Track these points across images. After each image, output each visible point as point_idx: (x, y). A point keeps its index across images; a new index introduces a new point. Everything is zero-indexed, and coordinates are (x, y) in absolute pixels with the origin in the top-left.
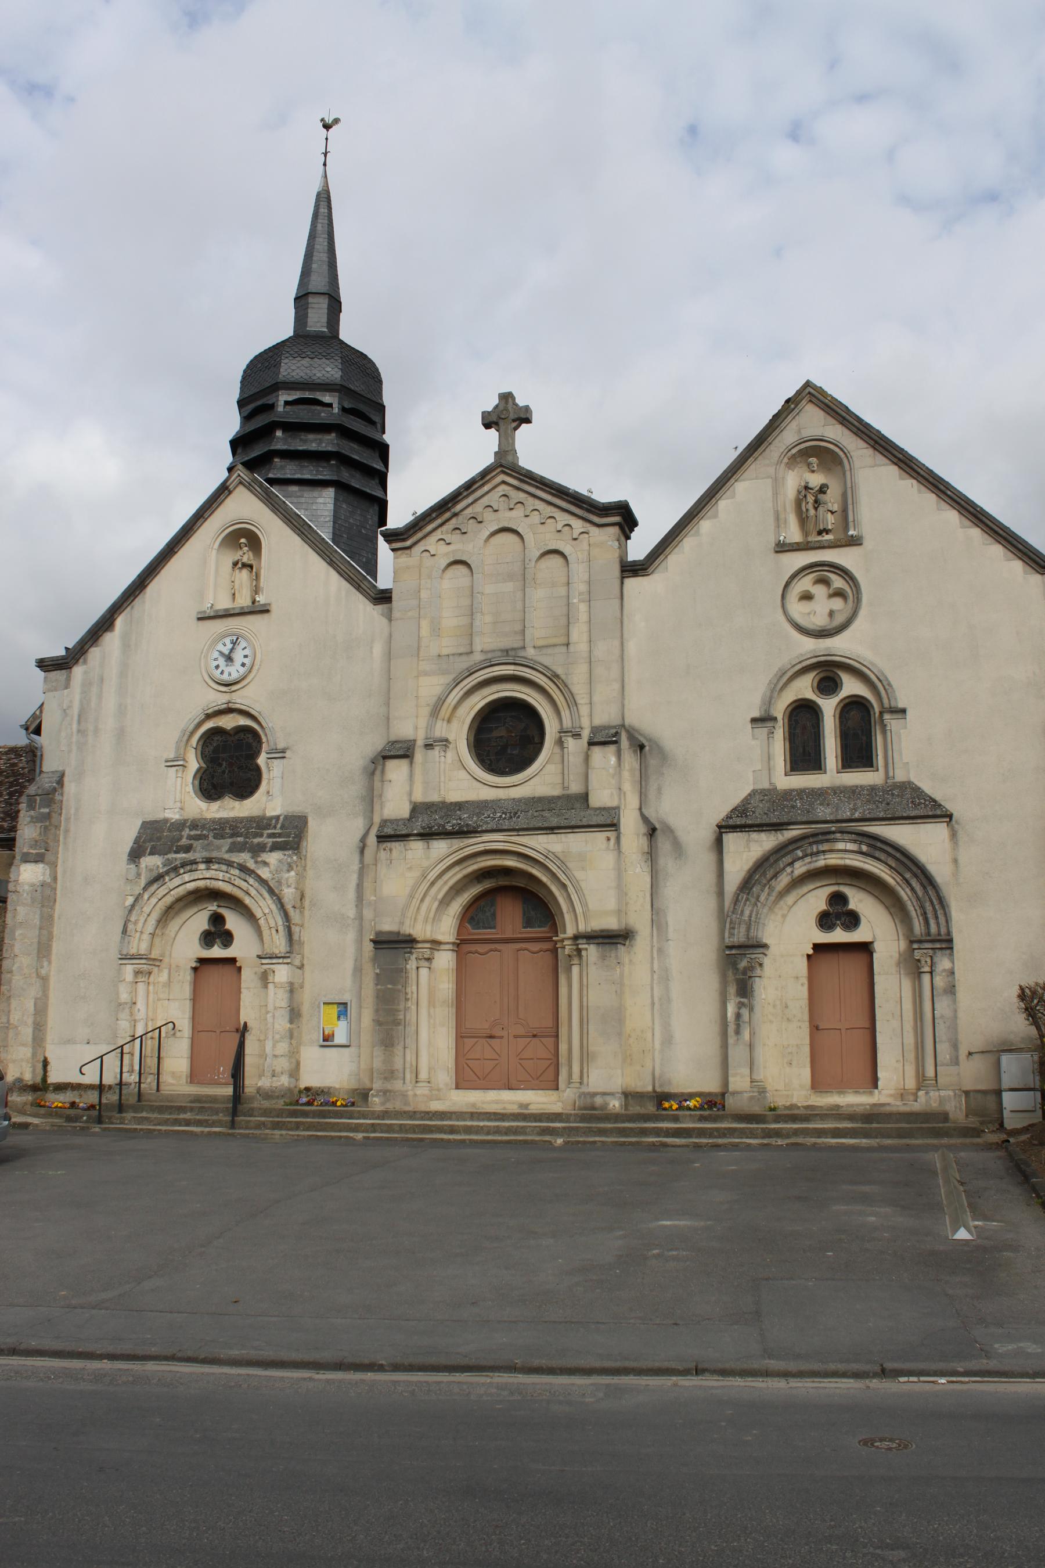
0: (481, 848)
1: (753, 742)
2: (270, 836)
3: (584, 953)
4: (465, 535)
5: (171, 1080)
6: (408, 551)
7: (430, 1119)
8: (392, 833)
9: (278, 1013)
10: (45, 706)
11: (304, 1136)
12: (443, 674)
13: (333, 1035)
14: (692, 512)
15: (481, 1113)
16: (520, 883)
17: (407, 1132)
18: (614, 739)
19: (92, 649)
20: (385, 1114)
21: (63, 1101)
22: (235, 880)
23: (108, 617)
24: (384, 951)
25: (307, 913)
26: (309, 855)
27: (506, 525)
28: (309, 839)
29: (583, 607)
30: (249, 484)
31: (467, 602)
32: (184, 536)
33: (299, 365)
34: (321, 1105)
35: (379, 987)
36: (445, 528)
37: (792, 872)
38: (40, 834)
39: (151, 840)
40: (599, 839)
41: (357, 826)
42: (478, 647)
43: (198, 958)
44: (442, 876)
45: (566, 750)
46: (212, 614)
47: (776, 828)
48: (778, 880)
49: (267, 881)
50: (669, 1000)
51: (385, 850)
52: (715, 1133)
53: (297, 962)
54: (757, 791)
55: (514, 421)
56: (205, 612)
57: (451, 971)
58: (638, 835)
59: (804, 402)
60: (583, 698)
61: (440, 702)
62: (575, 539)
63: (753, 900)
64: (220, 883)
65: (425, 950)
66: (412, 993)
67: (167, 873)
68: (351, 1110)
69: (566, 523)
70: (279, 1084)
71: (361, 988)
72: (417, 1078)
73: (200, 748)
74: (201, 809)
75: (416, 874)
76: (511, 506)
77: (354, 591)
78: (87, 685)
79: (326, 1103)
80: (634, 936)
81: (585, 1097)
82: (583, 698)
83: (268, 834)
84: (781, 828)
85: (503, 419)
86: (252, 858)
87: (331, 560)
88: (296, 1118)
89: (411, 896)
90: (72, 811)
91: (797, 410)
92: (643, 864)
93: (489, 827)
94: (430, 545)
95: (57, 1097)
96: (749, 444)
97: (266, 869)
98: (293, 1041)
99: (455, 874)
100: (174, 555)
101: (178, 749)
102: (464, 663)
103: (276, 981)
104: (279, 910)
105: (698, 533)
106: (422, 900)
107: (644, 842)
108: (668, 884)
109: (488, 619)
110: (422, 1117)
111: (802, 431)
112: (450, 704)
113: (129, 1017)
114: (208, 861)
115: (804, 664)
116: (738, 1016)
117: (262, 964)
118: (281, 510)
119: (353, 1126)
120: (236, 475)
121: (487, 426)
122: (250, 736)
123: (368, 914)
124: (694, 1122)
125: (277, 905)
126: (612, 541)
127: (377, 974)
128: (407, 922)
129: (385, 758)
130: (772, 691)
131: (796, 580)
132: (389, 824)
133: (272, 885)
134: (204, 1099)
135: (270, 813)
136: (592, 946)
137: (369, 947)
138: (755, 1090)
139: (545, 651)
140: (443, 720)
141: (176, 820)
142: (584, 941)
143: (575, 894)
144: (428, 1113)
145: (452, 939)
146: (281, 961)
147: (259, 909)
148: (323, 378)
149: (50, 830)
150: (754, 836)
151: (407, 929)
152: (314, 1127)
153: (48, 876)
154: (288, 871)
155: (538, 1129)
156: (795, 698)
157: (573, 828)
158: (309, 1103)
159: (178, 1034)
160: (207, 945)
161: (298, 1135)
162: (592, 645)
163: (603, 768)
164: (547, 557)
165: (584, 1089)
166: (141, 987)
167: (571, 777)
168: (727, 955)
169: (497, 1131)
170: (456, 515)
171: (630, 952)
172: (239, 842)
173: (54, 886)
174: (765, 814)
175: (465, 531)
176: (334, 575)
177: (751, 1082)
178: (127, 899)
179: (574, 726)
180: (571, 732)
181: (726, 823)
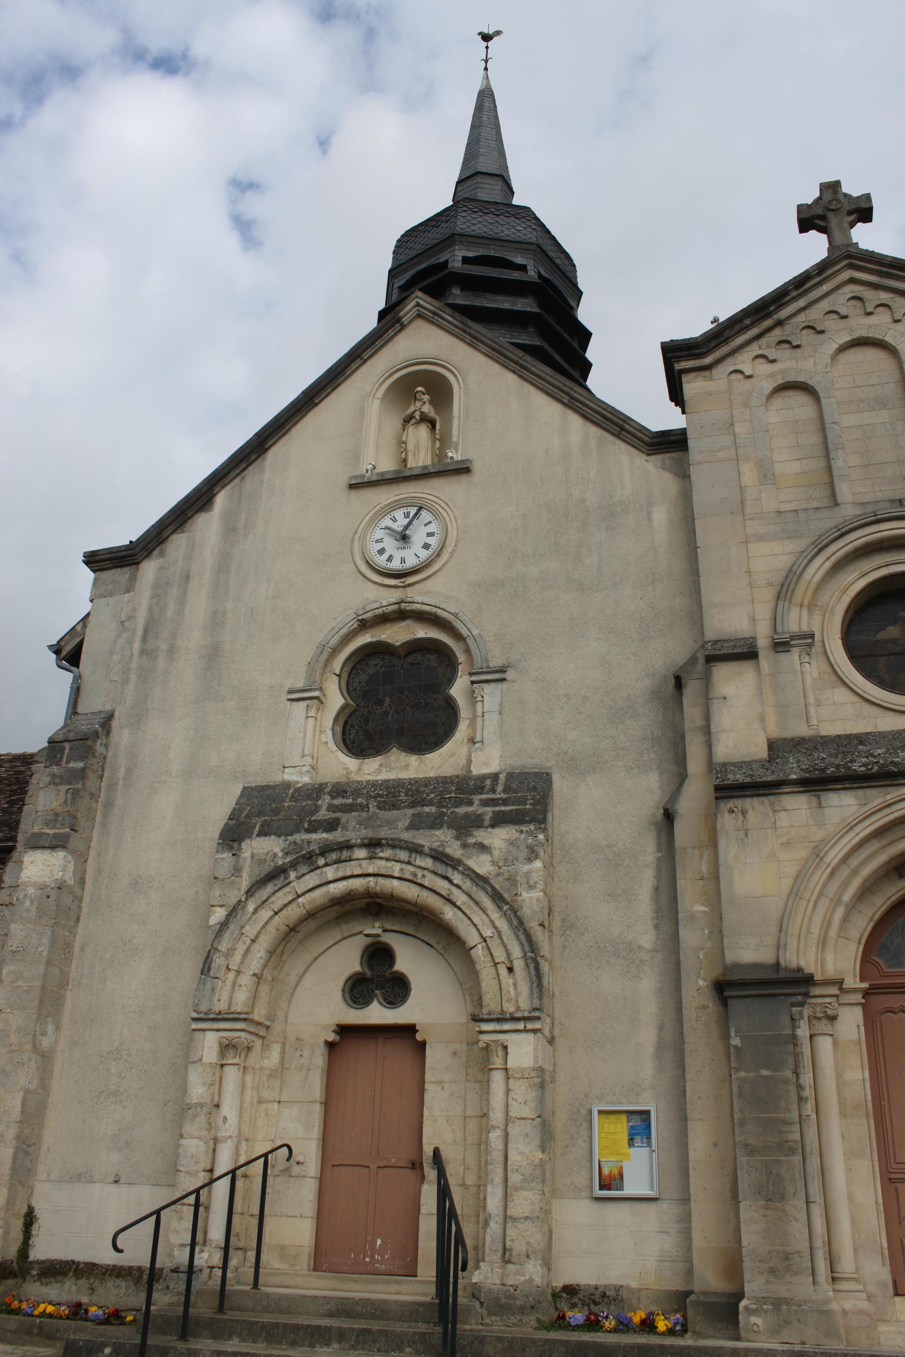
2: (485, 803)
4: (798, 351)
5: (277, 1264)
6: (707, 373)
8: (748, 780)
10: (90, 618)
12: (789, 538)
13: (621, 1175)
19: (175, 537)
21: (56, 1300)
22: (424, 876)
23: (205, 489)
27: (864, 333)
30: (434, 313)
31: (815, 439)
32: (331, 381)
33: (480, 220)
36: (764, 341)
38: (65, 802)
39: (259, 815)
42: (845, 492)
43: (338, 1025)
46: (374, 478)
55: (850, 213)
56: (363, 476)
64: (395, 883)
65: (827, 1000)
67: (294, 865)
70: (522, 1278)
72: (832, 1272)
73: (345, 676)
74: (347, 769)
75: (801, 853)
76: (869, 310)
77: (611, 438)
78: (160, 588)
83: (481, 800)
86: (457, 838)
87: (572, 397)
90: (122, 773)
95: (44, 1290)
97: (485, 858)
100: (313, 407)
101: (310, 673)
102: (827, 521)
113: (204, 1133)
114: (373, 844)
117: (481, 1032)
118: (485, 340)
120: (413, 303)
121: (805, 224)
122: (433, 657)
128: (792, 945)
129: (711, 659)
133: (497, 886)
134: (358, 1309)
135: (477, 770)
140: (801, 606)
141: (305, 785)
146: (520, 1026)
147: (473, 931)
148: (513, 236)
149: (82, 797)
153: (71, 875)
154: (530, 860)
159: (296, 1170)
160: (355, 1002)
166: (232, 1075)
170: (780, 323)
172: (428, 814)
173: (79, 894)
175: (798, 343)
178: (214, 912)
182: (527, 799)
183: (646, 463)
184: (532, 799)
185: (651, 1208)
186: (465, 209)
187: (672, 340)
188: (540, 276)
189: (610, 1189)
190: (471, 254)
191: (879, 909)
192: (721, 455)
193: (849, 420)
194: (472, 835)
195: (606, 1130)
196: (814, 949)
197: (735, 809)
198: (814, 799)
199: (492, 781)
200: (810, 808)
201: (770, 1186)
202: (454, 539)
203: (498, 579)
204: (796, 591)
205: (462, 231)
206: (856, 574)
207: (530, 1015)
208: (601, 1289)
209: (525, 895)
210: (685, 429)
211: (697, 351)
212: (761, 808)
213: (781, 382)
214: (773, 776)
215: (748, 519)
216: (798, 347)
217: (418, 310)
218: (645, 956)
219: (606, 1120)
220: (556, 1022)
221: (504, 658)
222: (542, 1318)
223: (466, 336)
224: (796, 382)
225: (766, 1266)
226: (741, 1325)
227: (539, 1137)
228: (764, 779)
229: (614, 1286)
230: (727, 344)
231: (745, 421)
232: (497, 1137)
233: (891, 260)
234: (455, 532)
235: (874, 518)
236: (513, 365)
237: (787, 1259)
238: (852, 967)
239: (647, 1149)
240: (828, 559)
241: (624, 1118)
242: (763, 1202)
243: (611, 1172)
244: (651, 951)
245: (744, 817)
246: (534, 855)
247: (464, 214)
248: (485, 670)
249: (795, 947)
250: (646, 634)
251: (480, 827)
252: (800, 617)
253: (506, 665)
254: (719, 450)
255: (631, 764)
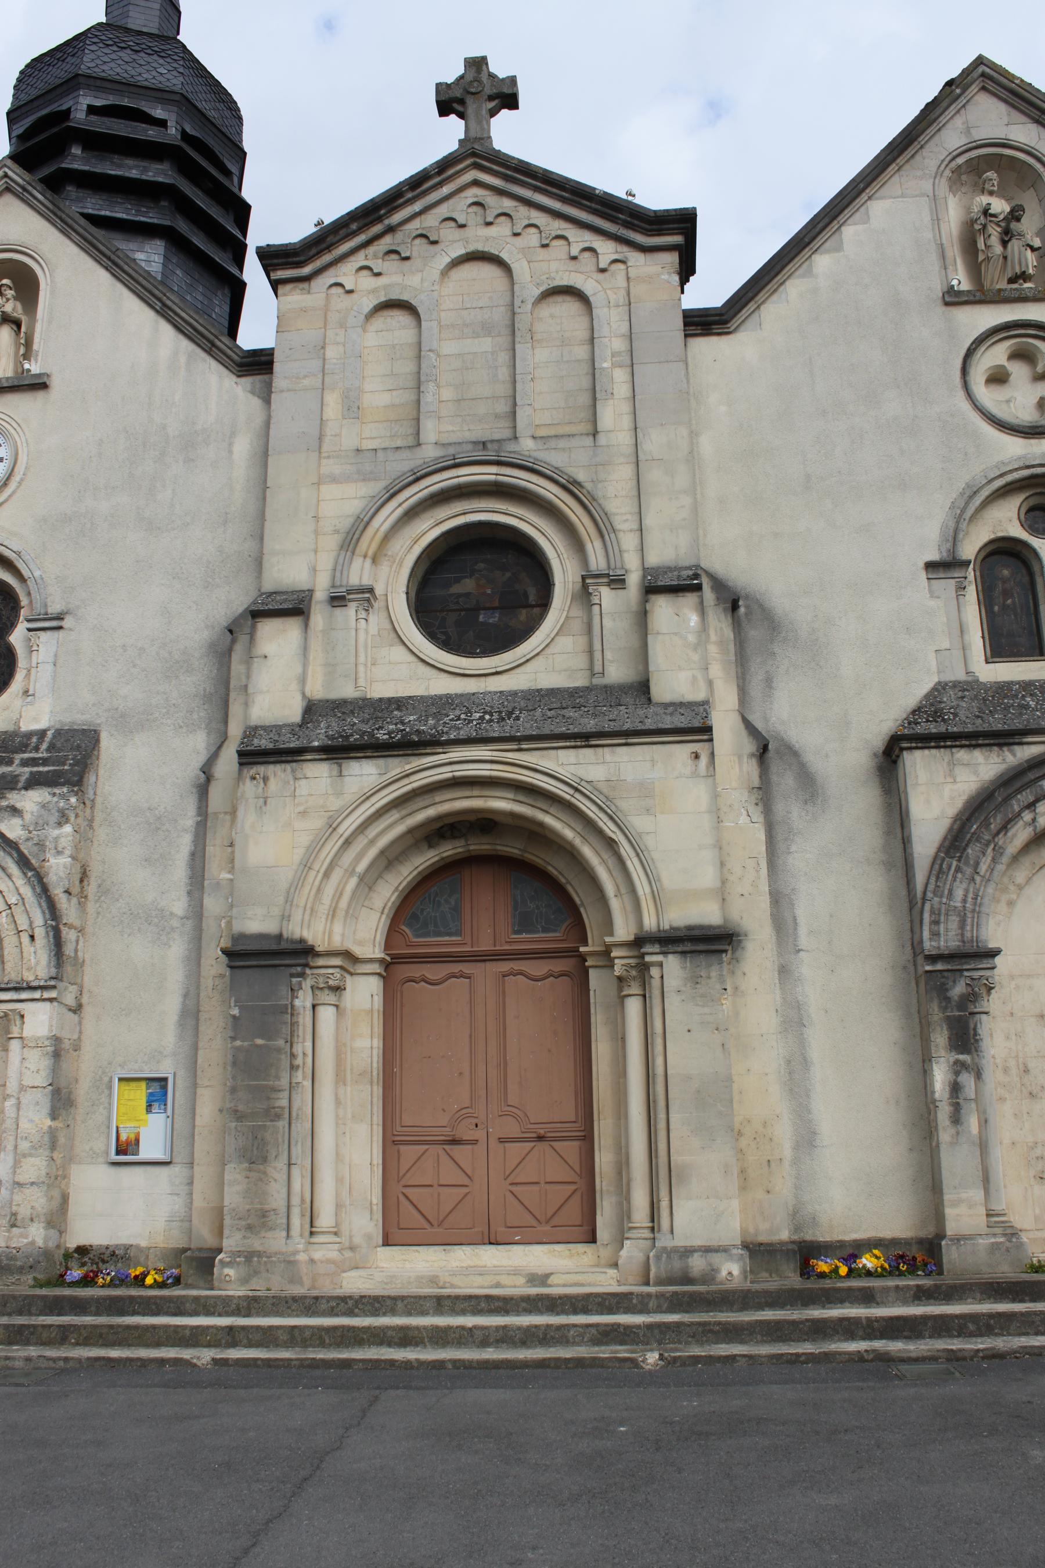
0: (445, 773)
1: (932, 603)
2: (25, 763)
3: (655, 972)
4: (407, 263)
6: (305, 285)
7: (350, 1313)
8: (271, 746)
9: (27, 1098)
11: (79, 1360)
12: (364, 480)
13: (137, 1141)
14: (802, 239)
15: (457, 1297)
16: (511, 848)
17: (305, 1344)
18: (695, 582)
20: (251, 1305)
24: (249, 971)
25: (91, 907)
26: (99, 800)
27: (480, 247)
28: (101, 772)
29: (620, 376)
30: (24, 189)
31: (410, 367)
33: (113, 56)
34: (112, 1285)
35: (238, 1043)
36: (371, 250)
37: (1034, 820)
40: (680, 753)
41: (199, 743)
42: (430, 431)
44: (366, 828)
45: (596, 608)
47: (1001, 741)
48: (1010, 834)
49: (16, 844)
50: (806, 1063)
51: (253, 778)
52: (971, 1327)
53: (70, 999)
54: (946, 684)
55: (491, 98)
57: (376, 1015)
58: (740, 757)
59: (974, 88)
60: (627, 520)
61: (361, 524)
62: (603, 271)
63: (969, 871)
65: (330, 971)
66: (304, 1054)
68: (179, 1297)
69: (586, 245)
70: (25, 1241)
71: (195, 1048)
72: (312, 1226)
75: (317, 823)
76: (490, 219)
77: (202, 354)
79: (121, 1281)
80: (740, 941)
81: (669, 1257)
82: (627, 520)
83: (22, 759)
84: (1011, 741)
85: (473, 94)
87: (164, 304)
88: (59, 1314)
89: (306, 865)
91: (963, 100)
92: (752, 809)
93: (463, 734)
94: (345, 274)
96: (890, 144)
97: (16, 821)
98: (56, 1155)
99: (391, 826)
102: (403, 464)
103: (24, 1035)
104: (38, 896)
105: (809, 273)
106: (327, 875)
107: (752, 768)
108: (793, 848)
109: (447, 394)
110: (333, 1308)
111: (973, 131)
112: (378, 530)
115: (1009, 478)
116: (955, 1088)
118: (76, 227)
119: (187, 1332)
121: (445, 108)
123: (213, 905)
124: (905, 1302)
125: (34, 889)
126: (669, 274)
127: (234, 1017)
128: (297, 915)
130: (958, 520)
131: (983, 348)
132: (262, 732)
133: (26, 852)
135: (26, 726)
136: (671, 957)
137: (214, 964)
138: (998, 1231)
139: (553, 443)
140: (365, 557)
142: (656, 948)
143: (636, 860)
144: (344, 1299)
145: (379, 954)
146: (37, 995)
148: (154, 81)
150: (961, 754)
151: (299, 929)
152: (101, 1335)
154: (60, 824)
155: (593, 1331)
156: (993, 536)
157: (628, 736)
158: (87, 1281)
161: (66, 1359)
162: (640, 435)
163: (676, 634)
164: (551, 299)
165: (664, 1241)
167: (608, 655)
168: (927, 972)
169: (505, 1337)
170: (391, 230)
171: (733, 973)
174: (978, 717)
175: (407, 254)
176: (167, 330)
177: (988, 1215)
179: (612, 566)
180: (608, 575)
181: (911, 732)
182: (68, 760)
183: (235, 386)
184: (72, 759)
185: (163, 1171)
186: (95, 40)
187: (268, 245)
188: (184, 133)
189: (126, 1155)
190: (98, 103)
191: (405, 878)
192: (306, 382)
193: (449, 348)
194: (5, 797)
195: (126, 1097)
196: (323, 920)
197: (257, 776)
198: (335, 767)
199: (38, 739)
200: (331, 777)
201: (255, 1149)
202: (24, 467)
203: (65, 514)
204: (362, 540)
205: (88, 71)
206: (431, 522)
207: (45, 984)
208: (111, 1249)
209: (53, 861)
210: (273, 349)
211: (295, 259)
212: (283, 776)
213: (383, 299)
214: (297, 743)
215: (325, 458)
216: (407, 258)
217: (6, 182)
218: (175, 923)
219: (125, 1086)
220: (85, 991)
221: (64, 604)
222: (39, 1277)
223: (57, 220)
224: (399, 300)
225: (244, 1223)
226: (215, 1277)
227: (49, 1105)
228: (287, 746)
229: (124, 1245)
230: (330, 251)
231: (338, 343)
232: (12, 1105)
233: (516, 162)
234: (25, 458)
235: (414, 477)
236: (105, 260)
237: (264, 1216)
238: (373, 937)
239: (163, 1115)
240: (400, 505)
241: (143, 1085)
242: (247, 1165)
243: (128, 1137)
244: (182, 919)
245: (265, 784)
246: (64, 819)
247: (94, 47)
248: (41, 616)
249: (300, 917)
250: (211, 580)
251: (13, 789)
252: (362, 569)
253: (65, 611)
254: (305, 377)
255: (180, 722)
